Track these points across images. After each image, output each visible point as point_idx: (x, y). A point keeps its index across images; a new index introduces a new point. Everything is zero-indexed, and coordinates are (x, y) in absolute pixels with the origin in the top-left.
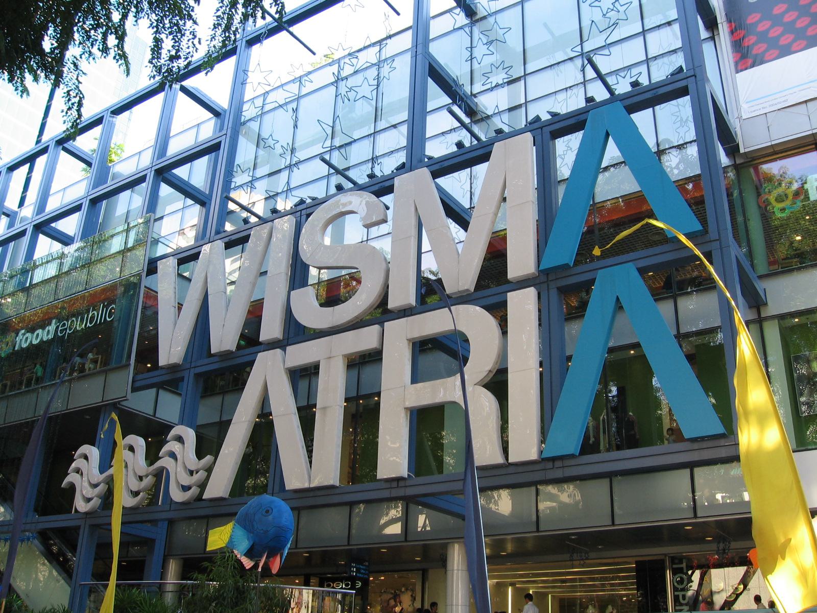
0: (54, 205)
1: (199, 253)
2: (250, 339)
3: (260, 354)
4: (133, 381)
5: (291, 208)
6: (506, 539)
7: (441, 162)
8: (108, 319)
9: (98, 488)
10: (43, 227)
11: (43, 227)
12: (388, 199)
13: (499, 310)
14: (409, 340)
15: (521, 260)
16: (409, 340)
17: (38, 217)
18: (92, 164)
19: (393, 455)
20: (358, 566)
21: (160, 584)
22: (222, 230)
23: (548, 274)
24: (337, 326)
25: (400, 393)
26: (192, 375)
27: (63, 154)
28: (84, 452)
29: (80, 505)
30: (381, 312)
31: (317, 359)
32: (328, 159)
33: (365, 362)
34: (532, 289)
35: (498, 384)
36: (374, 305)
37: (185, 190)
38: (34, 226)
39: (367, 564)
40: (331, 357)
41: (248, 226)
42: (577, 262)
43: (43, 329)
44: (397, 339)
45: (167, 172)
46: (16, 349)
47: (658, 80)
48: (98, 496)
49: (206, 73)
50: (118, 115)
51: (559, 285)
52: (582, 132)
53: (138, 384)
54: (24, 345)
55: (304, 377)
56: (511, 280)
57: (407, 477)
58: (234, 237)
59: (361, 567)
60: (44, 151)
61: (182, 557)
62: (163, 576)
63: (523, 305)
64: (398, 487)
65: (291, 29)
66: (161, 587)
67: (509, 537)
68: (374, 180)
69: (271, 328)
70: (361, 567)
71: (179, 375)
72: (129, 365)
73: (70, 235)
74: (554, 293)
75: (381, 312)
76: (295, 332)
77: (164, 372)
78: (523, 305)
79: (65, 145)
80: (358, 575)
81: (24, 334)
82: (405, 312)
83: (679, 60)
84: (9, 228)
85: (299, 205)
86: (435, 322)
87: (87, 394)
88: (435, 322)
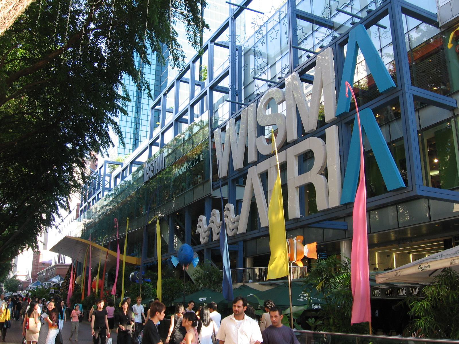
0: (217, 74)
1: (315, 61)
4: (213, 186)
5: (330, 42)
6: (407, 228)
7: (375, 13)
9: (206, 233)
10: (214, 88)
11: (214, 88)
12: (284, 89)
13: (323, 137)
14: (295, 156)
16: (295, 156)
17: (176, 116)
18: (229, 47)
20: (320, 253)
21: (243, 269)
22: (297, 65)
23: (341, 117)
26: (230, 180)
27: (181, 83)
28: (310, 182)
29: (202, 241)
31: (266, 169)
34: (334, 126)
35: (325, 172)
36: (283, 141)
37: (224, 90)
38: (209, 88)
39: (326, 252)
41: (310, 59)
42: (350, 111)
44: (291, 156)
45: (215, 87)
46: (176, 177)
48: (207, 237)
50: (195, 62)
51: (345, 122)
52: (388, 15)
53: (215, 187)
55: (264, 177)
56: (327, 122)
57: (299, 217)
58: (304, 68)
59: (322, 253)
60: (206, 48)
61: (253, 256)
62: (244, 265)
63: (332, 132)
64: (347, 208)
65: (248, 7)
66: (244, 271)
67: (392, 231)
68: (371, 13)
69: (252, 157)
70: (322, 253)
71: (226, 181)
74: (343, 125)
76: (261, 158)
77: (237, 172)
79: (181, 79)
80: (321, 257)
84: (191, 99)
85: (333, 40)
87: (198, 194)
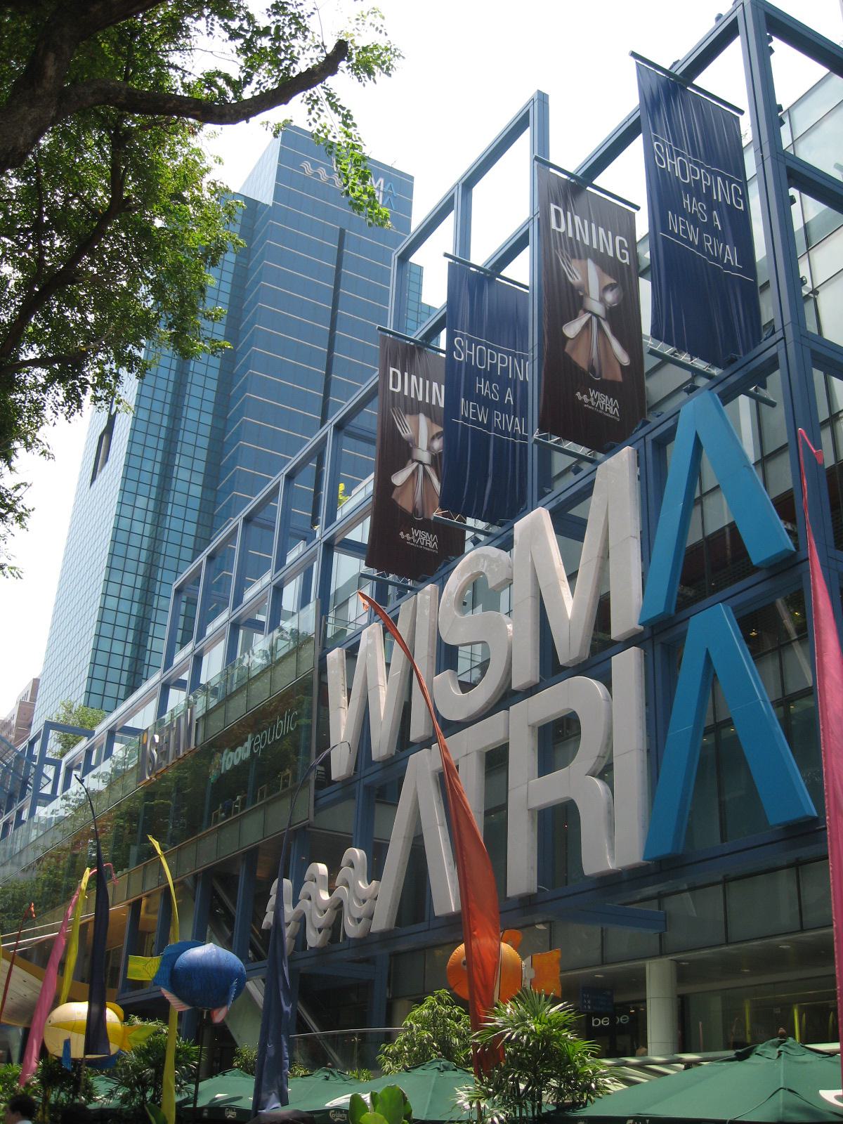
2: (404, 744)
3: (411, 757)
4: (316, 799)
8: (269, 743)
15: (625, 619)
19: (522, 874)
24: (638, 497)
25: (529, 790)
26: (362, 786)
30: (507, 698)
32: (647, 368)
33: (496, 760)
40: (466, 749)
43: (242, 745)
47: (351, 737)
49: (17, 457)
54: (228, 767)
63: (627, 665)
72: (309, 781)
73: (283, 604)
75: (507, 698)
77: (338, 786)
78: (627, 665)
81: (227, 754)
82: (531, 691)
83: (375, 582)
86: (548, 704)
88: (548, 704)
